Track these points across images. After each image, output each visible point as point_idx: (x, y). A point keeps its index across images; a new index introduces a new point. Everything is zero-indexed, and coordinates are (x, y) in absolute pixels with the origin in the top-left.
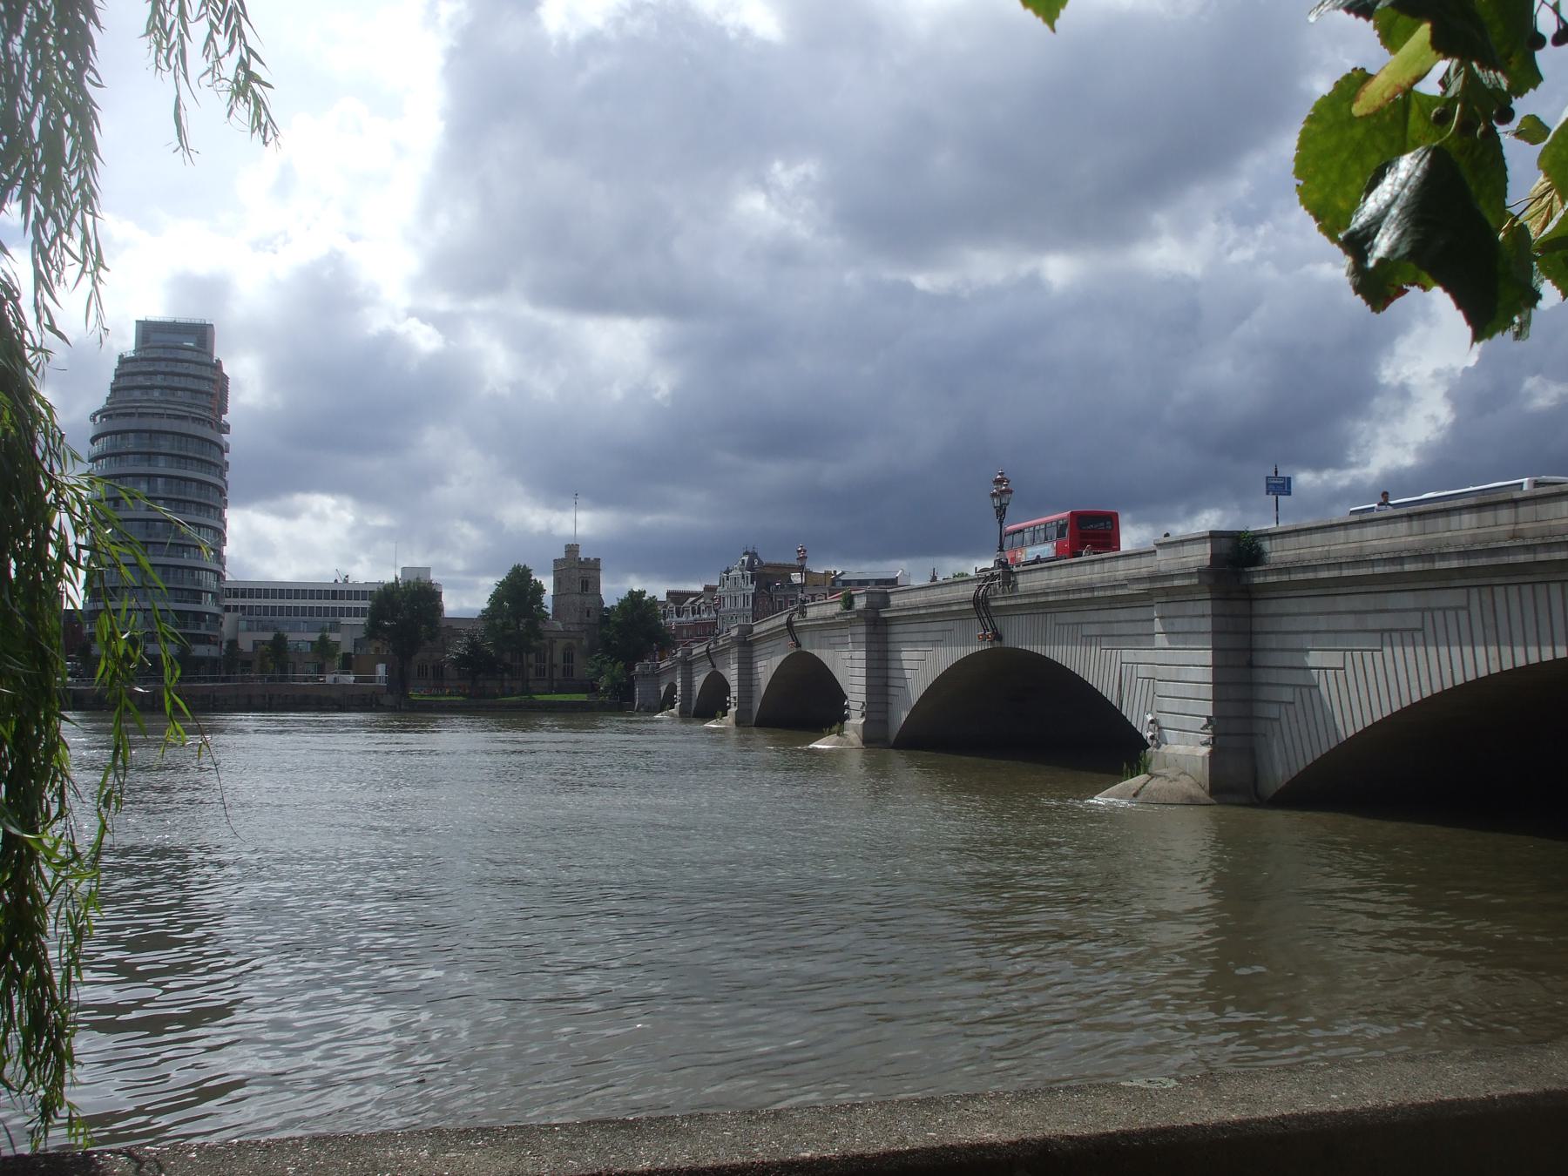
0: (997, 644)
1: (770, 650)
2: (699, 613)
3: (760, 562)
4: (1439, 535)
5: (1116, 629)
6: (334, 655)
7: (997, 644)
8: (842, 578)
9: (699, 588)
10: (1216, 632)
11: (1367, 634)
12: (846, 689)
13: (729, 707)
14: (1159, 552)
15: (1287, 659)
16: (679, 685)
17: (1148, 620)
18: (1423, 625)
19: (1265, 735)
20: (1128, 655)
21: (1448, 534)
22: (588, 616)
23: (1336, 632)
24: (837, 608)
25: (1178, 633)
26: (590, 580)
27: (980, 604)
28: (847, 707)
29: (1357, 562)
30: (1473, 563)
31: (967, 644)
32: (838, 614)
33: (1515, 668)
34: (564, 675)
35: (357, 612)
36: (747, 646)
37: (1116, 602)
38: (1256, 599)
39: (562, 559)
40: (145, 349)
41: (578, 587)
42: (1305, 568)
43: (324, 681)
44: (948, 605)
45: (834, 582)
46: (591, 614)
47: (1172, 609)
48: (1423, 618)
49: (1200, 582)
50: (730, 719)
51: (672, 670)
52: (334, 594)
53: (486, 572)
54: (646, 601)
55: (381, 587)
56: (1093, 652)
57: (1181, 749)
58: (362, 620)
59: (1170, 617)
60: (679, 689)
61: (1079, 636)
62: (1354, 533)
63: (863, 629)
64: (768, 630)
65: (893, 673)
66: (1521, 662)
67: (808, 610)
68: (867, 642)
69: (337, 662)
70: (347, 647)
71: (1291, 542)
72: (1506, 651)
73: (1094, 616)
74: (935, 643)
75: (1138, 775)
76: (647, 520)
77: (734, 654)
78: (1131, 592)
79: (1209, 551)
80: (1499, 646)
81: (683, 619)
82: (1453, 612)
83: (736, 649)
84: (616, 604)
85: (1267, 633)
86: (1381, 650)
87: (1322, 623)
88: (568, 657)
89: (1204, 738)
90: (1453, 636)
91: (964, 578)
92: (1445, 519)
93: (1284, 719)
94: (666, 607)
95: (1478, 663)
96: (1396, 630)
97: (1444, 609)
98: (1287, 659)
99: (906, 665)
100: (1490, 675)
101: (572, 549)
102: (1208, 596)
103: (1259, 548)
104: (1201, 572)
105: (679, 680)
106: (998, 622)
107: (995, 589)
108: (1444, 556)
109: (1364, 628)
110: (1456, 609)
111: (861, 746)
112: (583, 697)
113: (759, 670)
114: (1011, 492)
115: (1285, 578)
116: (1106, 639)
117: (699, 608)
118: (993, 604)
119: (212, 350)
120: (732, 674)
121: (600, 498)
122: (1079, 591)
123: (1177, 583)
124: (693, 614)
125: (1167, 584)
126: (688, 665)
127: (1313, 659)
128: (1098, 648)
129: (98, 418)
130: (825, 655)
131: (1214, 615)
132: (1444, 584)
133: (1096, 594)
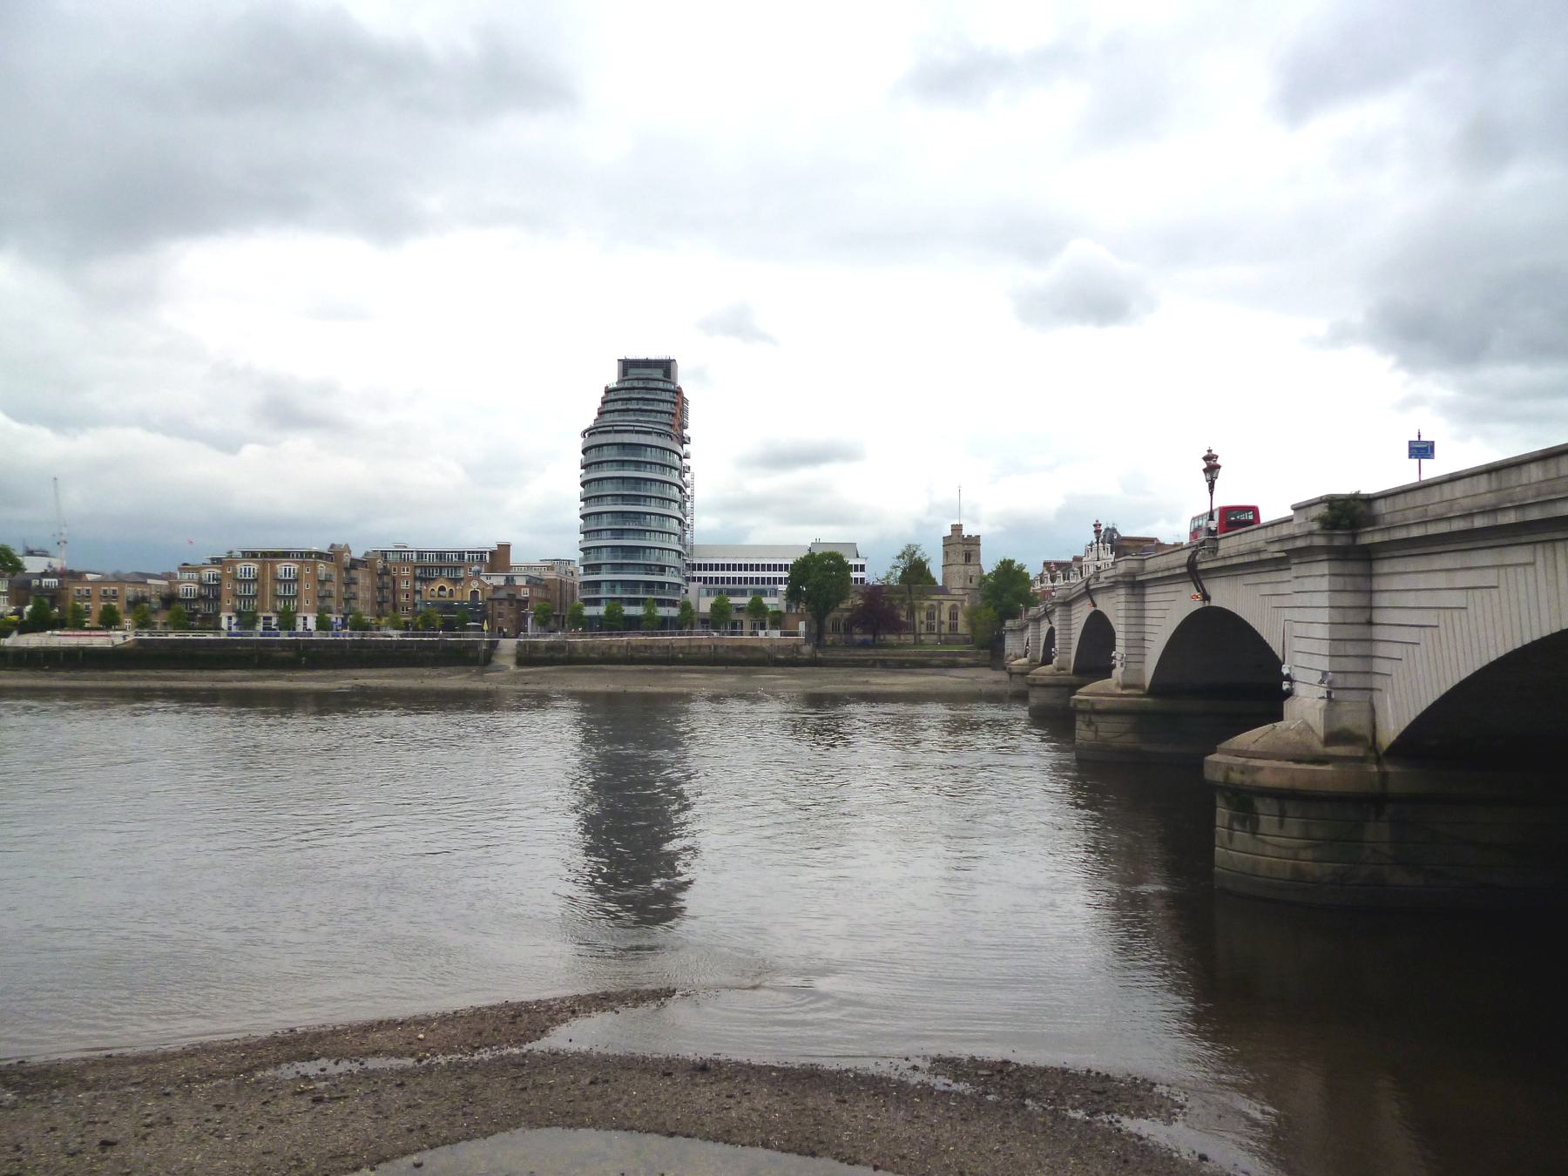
0: (1207, 604)
3: (1119, 535)
11: (1455, 591)
22: (971, 582)
26: (972, 553)
28: (1114, 658)
34: (950, 630)
40: (624, 381)
46: (973, 580)
48: (1499, 576)
91: (1179, 548)
93: (1394, 675)
102: (1325, 557)
109: (1453, 586)
117: (1069, 575)
118: (1092, 587)
119: (676, 378)
124: (1064, 580)
129: (586, 434)
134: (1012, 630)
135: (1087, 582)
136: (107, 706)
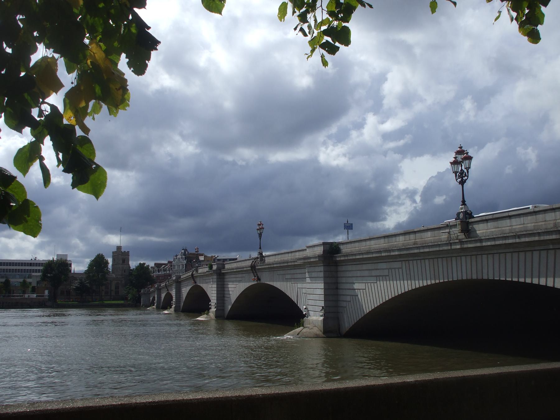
1: (186, 284)
2: (166, 271)
3: (188, 253)
4: (392, 244)
5: (296, 276)
6: (28, 287)
7: (259, 282)
8: (218, 258)
9: (166, 262)
10: (325, 277)
12: (211, 298)
13: (172, 305)
14: (307, 249)
15: (348, 286)
16: (156, 297)
17: (304, 273)
18: (389, 274)
19: (342, 313)
20: (300, 285)
21: (396, 243)
22: (125, 272)
23: (363, 277)
24: (207, 269)
25: (313, 277)
27: (253, 268)
28: (210, 305)
29: (368, 253)
30: (402, 253)
31: (250, 282)
32: (207, 271)
33: (420, 287)
35: (39, 271)
36: (179, 283)
37: (295, 267)
38: (339, 265)
39: (116, 251)
41: (121, 262)
42: (352, 255)
43: (24, 297)
44: (243, 268)
45: (214, 259)
47: (312, 269)
49: (319, 259)
50: (172, 309)
51: (154, 292)
52: (31, 264)
53: (88, 257)
54: (146, 267)
55: (47, 262)
56: (287, 284)
57: (314, 318)
58: (40, 274)
59: (311, 272)
60: (156, 299)
61: (285, 279)
62: (368, 243)
63: (215, 277)
64: (186, 277)
65: (226, 292)
66: (421, 285)
67: (199, 270)
68: (217, 281)
69: (30, 289)
70: (34, 284)
71: (349, 246)
72: (417, 282)
73: (289, 272)
74: (240, 281)
75: (300, 327)
76: (141, 238)
77: (174, 286)
78: (298, 263)
79: (322, 249)
80: (390, 281)
81: (160, 273)
82: (394, 270)
83: (175, 284)
84: (135, 268)
85: (342, 277)
86: (377, 283)
87: (359, 273)
88: (117, 287)
89: (321, 314)
90: (420, 277)
92: (395, 238)
93: (348, 307)
94: (154, 269)
95: (385, 288)
96: (381, 276)
97: (395, 269)
98: (348, 286)
99: (230, 289)
100: (405, 292)
101: (119, 248)
102: (322, 265)
103: (339, 248)
104: (319, 256)
105: (156, 295)
106: (259, 274)
107: (258, 262)
108: (393, 251)
110: (398, 268)
111: (215, 318)
112: (122, 302)
113: (183, 292)
114: (263, 228)
115: (346, 258)
116: (293, 279)
117: (166, 269)
118: (257, 268)
120: (173, 293)
121: (121, 230)
122: (284, 263)
123: (312, 260)
124: (164, 271)
125: (309, 261)
126: (159, 290)
127: (356, 286)
128: (290, 283)
130: (204, 286)
131: (324, 271)
132: (395, 260)
133: (289, 264)
134: (144, 294)
135: (192, 273)
136: (127, 310)
